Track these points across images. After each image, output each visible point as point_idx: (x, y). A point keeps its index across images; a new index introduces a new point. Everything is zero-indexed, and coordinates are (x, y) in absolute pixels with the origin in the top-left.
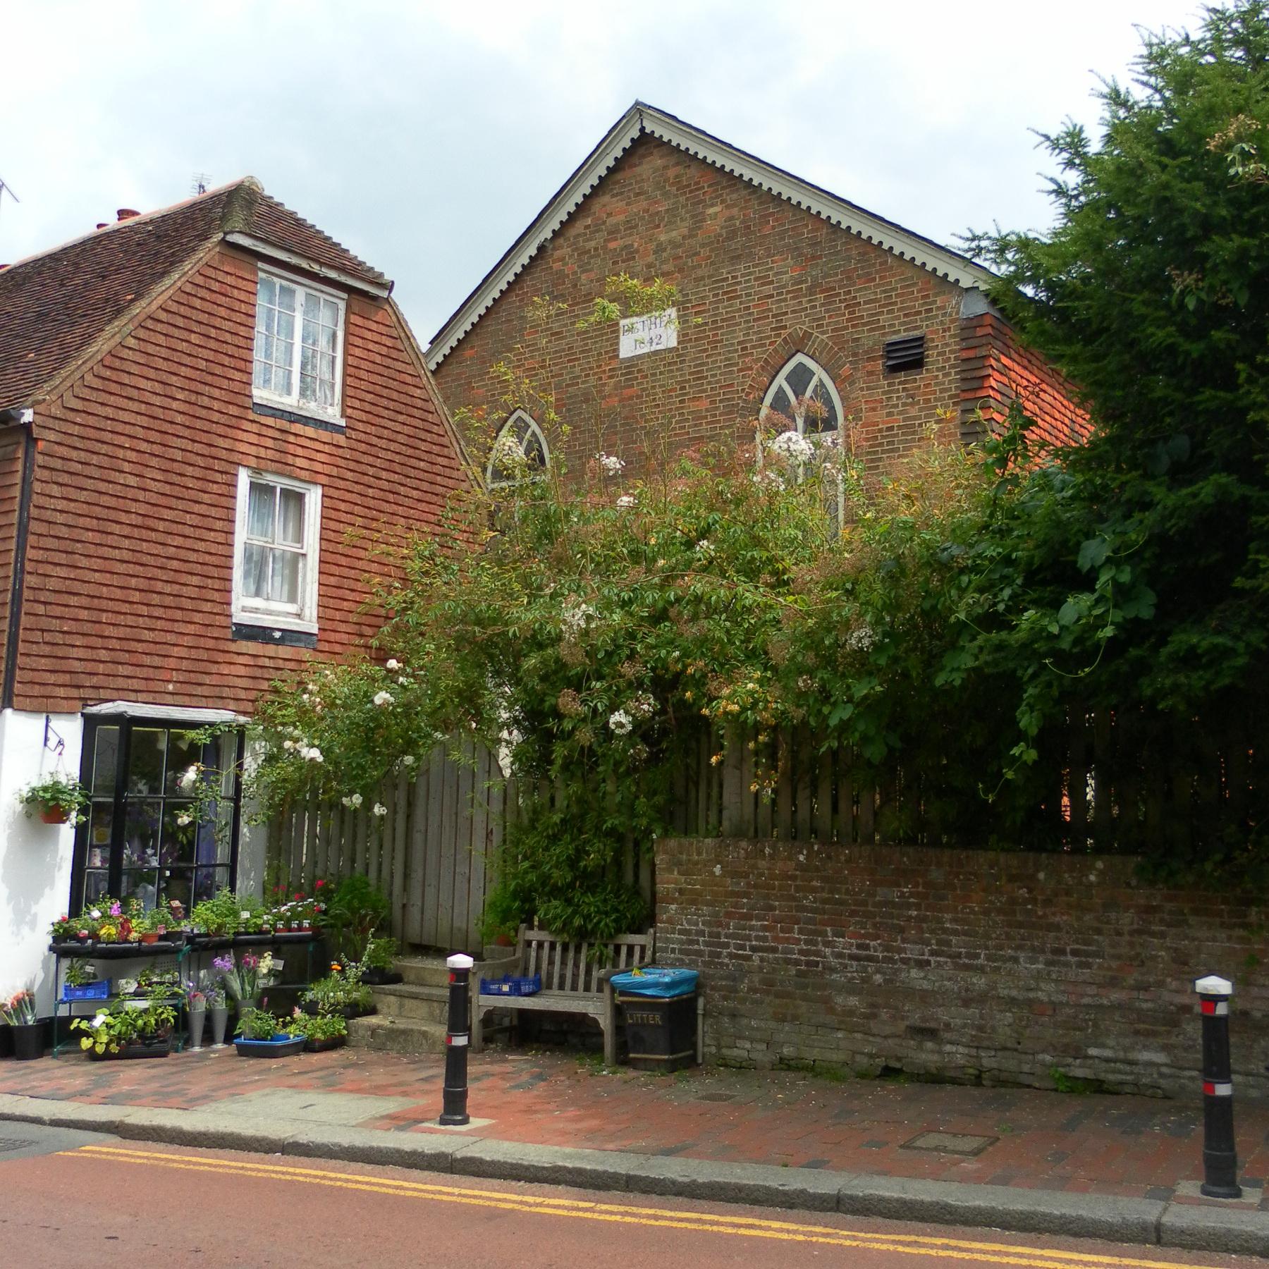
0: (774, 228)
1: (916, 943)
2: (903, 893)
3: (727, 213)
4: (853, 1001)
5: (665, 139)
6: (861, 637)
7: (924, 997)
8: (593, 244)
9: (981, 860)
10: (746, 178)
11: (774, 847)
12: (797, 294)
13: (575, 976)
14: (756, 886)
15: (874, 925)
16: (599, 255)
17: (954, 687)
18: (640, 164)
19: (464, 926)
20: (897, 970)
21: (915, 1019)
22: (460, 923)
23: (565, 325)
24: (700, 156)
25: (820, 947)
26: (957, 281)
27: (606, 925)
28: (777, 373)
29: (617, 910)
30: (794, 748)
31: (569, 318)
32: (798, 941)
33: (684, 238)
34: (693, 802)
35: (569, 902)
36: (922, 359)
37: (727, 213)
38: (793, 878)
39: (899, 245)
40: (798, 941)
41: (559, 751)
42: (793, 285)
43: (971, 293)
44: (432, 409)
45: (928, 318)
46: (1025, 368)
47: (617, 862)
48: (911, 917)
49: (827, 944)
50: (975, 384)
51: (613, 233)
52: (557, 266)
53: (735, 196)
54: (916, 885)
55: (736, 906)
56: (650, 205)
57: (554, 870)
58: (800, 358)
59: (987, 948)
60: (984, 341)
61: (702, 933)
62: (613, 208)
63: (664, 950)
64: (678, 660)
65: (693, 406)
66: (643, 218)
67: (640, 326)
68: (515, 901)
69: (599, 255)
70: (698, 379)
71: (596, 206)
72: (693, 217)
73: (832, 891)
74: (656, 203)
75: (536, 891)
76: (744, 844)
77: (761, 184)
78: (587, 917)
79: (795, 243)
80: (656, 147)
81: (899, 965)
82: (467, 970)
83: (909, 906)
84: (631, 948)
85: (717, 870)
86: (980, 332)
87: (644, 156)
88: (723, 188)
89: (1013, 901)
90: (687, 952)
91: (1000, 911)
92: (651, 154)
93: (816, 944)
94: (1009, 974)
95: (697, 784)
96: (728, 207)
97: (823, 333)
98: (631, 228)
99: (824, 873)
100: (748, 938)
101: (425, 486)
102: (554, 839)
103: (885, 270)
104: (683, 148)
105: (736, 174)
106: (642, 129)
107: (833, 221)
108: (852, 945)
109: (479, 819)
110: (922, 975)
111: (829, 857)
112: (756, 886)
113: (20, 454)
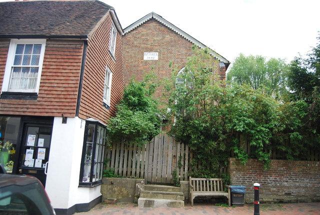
4: (274, 189)
7: (288, 188)
13: (200, 188)
21: (287, 192)
52: (128, 39)
61: (241, 177)
65: (161, 72)
71: (139, 29)
89: (303, 169)
106: (153, 17)
113: (83, 48)
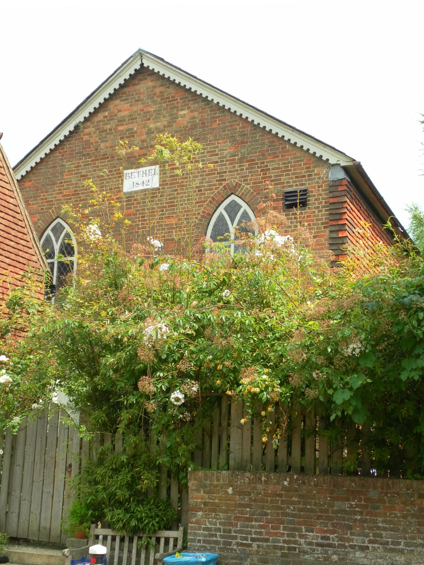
0: (219, 124)
1: (359, 535)
2: (351, 505)
3: (192, 115)
5: (156, 71)
6: (354, 348)
8: (108, 127)
9: (402, 485)
10: (204, 96)
11: (267, 477)
12: (232, 162)
14: (255, 501)
15: (333, 525)
16: (112, 133)
17: (414, 380)
18: (138, 84)
19: (48, 526)
20: (347, 552)
22: (45, 524)
23: (90, 172)
24: (177, 82)
25: (297, 538)
26: (328, 160)
27: (153, 525)
28: (219, 205)
29: (158, 516)
30: (303, 416)
31: (93, 167)
32: (283, 535)
33: (165, 127)
34: (207, 449)
35: (127, 510)
36: (306, 201)
37: (192, 115)
38: (280, 495)
39: (294, 138)
40: (283, 535)
41: (125, 416)
42: (230, 157)
43: (335, 167)
44: (19, 212)
45: (309, 180)
46: (359, 211)
47: (158, 487)
48: (356, 520)
49: (301, 536)
50: (338, 217)
51: (121, 121)
52: (86, 138)
53: (196, 106)
54: (360, 500)
55: (242, 513)
56: (145, 107)
57: (118, 491)
58: (233, 197)
59: (405, 539)
60: (343, 193)
61: (219, 530)
62: (122, 107)
63: (193, 541)
64: (211, 361)
65: (167, 221)
66: (140, 114)
67: (136, 174)
68: (88, 510)
69: (112, 133)
70: (172, 206)
71: (111, 106)
72: (170, 115)
73: (305, 504)
74: (148, 106)
75: (104, 503)
76: (248, 474)
77: (213, 100)
78: (140, 520)
79: (231, 134)
80: (148, 75)
81: (349, 549)
82: (103, 556)
83: (355, 513)
84: (167, 540)
85: (230, 490)
86: (340, 188)
87: (141, 80)
88: (189, 101)
90: (209, 542)
91: (413, 516)
92: (146, 79)
93: (294, 536)
94: (419, 554)
95: (211, 437)
96: (191, 111)
97: (248, 184)
98: (132, 119)
99: (300, 493)
100: (250, 533)
101: (13, 256)
102: (116, 471)
103: (285, 152)
104: (166, 76)
105: (198, 93)
106: (142, 65)
107: (256, 123)
108: (318, 537)
109: (61, 457)
110: (363, 555)
111: (304, 483)
112: (255, 501)
